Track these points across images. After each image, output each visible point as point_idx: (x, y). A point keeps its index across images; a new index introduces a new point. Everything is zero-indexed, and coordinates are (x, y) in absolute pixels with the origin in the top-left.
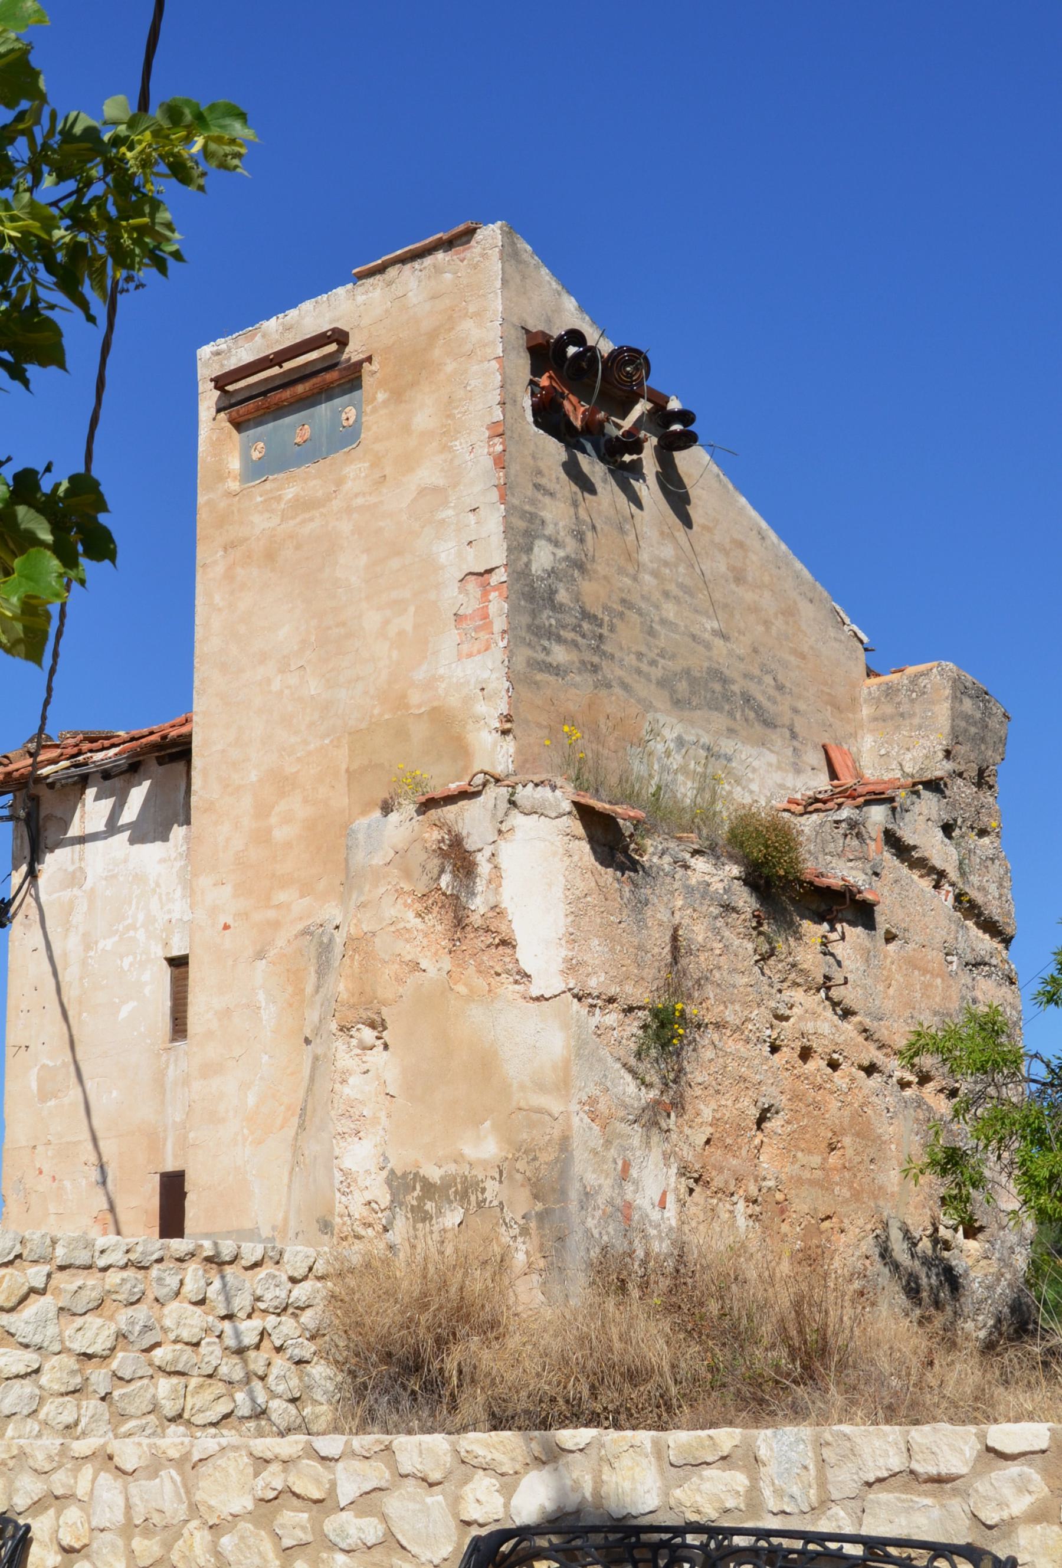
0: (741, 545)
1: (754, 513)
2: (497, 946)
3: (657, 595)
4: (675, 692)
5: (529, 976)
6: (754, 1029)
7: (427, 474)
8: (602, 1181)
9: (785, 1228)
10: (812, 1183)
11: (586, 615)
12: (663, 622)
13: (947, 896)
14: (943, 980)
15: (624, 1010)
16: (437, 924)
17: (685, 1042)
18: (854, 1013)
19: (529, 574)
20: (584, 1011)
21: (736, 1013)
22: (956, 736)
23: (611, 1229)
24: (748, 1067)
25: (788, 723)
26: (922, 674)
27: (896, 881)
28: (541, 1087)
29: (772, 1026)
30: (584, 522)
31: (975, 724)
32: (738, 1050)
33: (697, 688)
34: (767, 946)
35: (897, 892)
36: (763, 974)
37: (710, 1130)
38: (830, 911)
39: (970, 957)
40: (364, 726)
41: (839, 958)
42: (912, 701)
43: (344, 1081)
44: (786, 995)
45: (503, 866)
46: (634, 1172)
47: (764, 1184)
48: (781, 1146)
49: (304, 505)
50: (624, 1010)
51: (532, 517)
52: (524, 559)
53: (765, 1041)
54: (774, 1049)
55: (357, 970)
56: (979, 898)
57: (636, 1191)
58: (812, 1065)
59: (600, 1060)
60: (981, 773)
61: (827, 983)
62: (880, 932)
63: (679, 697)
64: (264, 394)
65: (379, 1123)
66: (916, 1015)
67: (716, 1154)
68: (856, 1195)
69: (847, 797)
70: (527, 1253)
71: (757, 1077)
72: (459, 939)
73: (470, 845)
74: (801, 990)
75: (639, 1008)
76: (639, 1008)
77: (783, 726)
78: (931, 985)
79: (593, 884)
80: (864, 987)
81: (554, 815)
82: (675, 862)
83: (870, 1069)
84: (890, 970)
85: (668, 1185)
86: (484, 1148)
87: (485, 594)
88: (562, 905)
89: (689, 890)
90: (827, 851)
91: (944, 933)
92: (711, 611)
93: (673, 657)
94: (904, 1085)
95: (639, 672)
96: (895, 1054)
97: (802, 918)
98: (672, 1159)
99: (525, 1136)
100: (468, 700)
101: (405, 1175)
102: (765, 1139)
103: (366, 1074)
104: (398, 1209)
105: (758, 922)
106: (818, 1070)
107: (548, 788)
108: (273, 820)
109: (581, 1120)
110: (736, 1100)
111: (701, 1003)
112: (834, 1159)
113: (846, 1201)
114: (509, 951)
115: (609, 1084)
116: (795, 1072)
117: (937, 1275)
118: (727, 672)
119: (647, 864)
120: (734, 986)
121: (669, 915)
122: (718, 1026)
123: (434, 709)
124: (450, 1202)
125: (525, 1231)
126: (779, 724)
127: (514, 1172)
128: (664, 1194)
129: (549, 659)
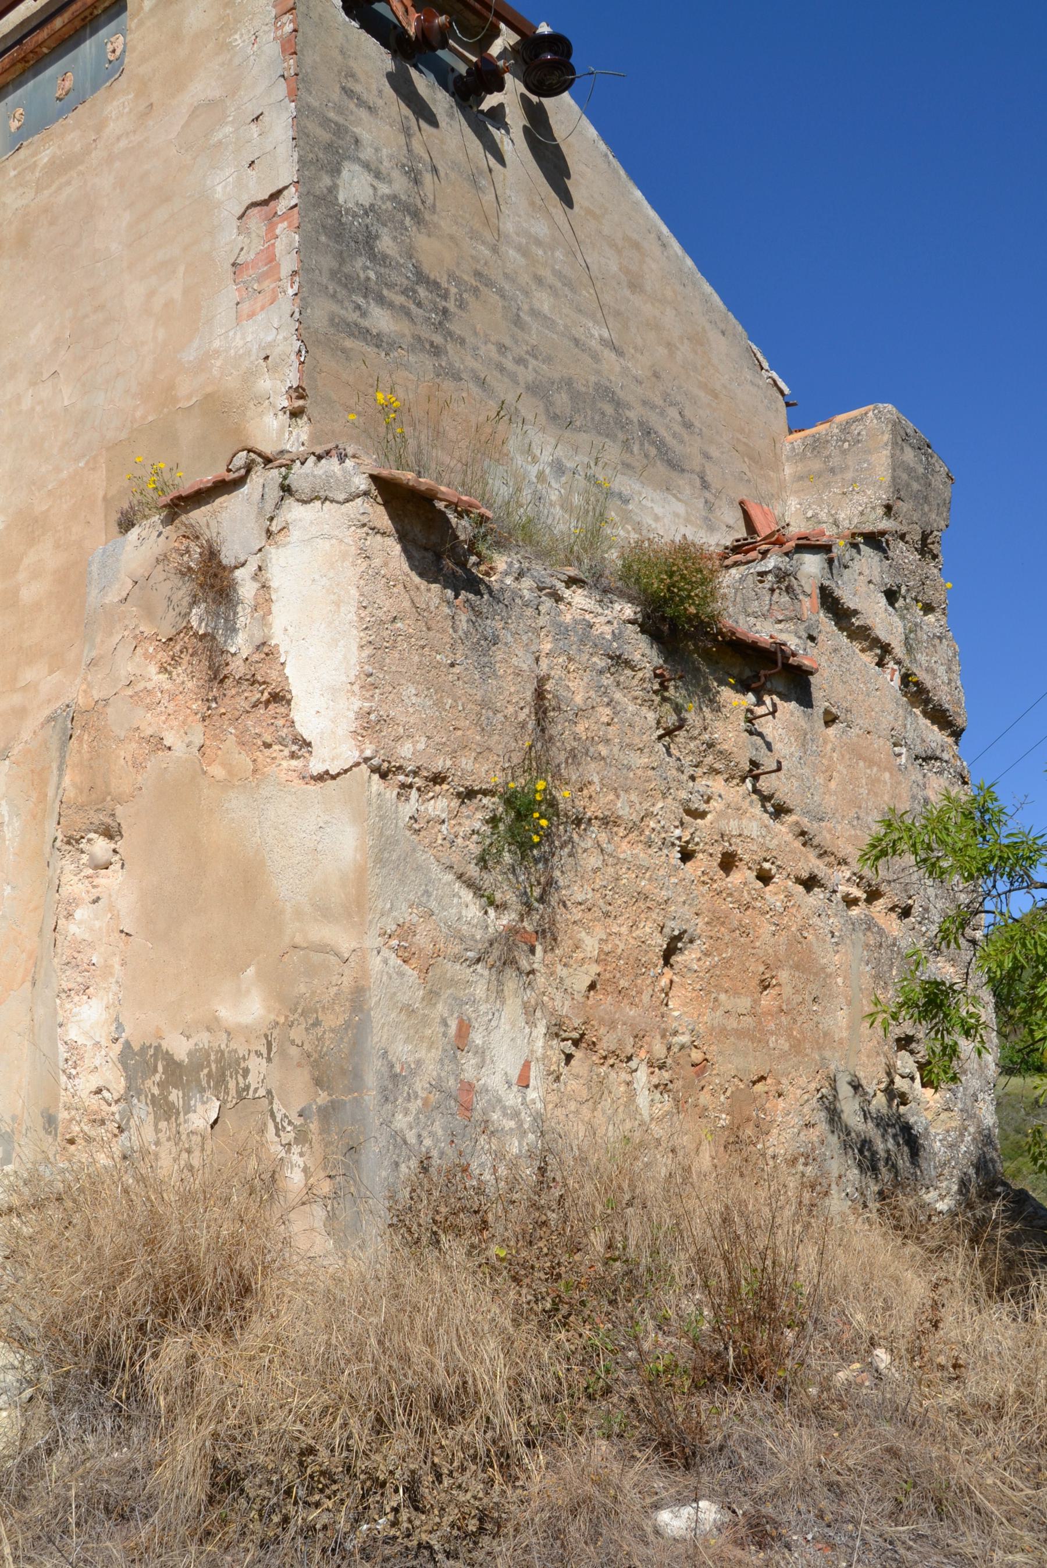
0: (636, 246)
1: (652, 213)
2: (267, 703)
3: (525, 278)
4: (552, 404)
5: (309, 745)
6: (658, 827)
7: (202, 87)
8: (422, 1054)
9: (704, 1098)
10: (740, 1034)
11: (421, 277)
12: (534, 313)
13: (893, 675)
14: (891, 774)
15: (459, 795)
16: (187, 679)
17: (557, 843)
18: (788, 811)
19: (335, 202)
20: (391, 794)
21: (632, 804)
22: (898, 490)
23: (438, 1128)
24: (650, 879)
25: (698, 469)
26: (856, 420)
27: (835, 650)
28: (324, 912)
29: (682, 824)
30: (420, 159)
31: (917, 479)
32: (635, 856)
33: (581, 405)
34: (675, 717)
35: (837, 666)
36: (669, 754)
37: (595, 969)
38: (757, 677)
39: (919, 750)
40: (123, 435)
41: (769, 739)
42: (844, 452)
43: (69, 916)
44: (701, 784)
45: (274, 584)
46: (477, 1038)
47: (675, 1040)
48: (698, 987)
49: (60, 167)
50: (459, 795)
51: (340, 131)
52: (327, 181)
53: (673, 844)
54: (687, 856)
55: (86, 756)
56: (929, 683)
57: (481, 1066)
58: (736, 877)
59: (418, 869)
60: (925, 537)
61: (754, 771)
62: (818, 711)
63: (558, 411)
64: (19, 42)
65: (112, 974)
66: (862, 815)
67: (604, 1002)
68: (797, 1047)
69: (773, 543)
70: (305, 1170)
71: (663, 893)
72: (215, 699)
73: (227, 558)
74: (720, 779)
75: (485, 793)
76: (485, 793)
77: (692, 472)
78: (878, 780)
79: (407, 604)
80: (800, 778)
81: (341, 497)
82: (541, 589)
83: (810, 883)
84: (831, 758)
85: (532, 1051)
86: (247, 1009)
87: (271, 226)
88: (355, 632)
89: (562, 631)
90: (750, 611)
91: (891, 718)
92: (599, 315)
93: (548, 360)
94: (850, 902)
95: (501, 369)
96: (839, 864)
97: (722, 682)
98: (538, 1014)
99: (302, 988)
100: (249, 377)
101: (144, 1049)
102: (675, 978)
103: (104, 899)
104: (135, 1101)
105: (661, 684)
106: (745, 884)
107: (335, 460)
108: (22, 576)
109: (386, 962)
110: (634, 925)
111: (581, 790)
112: (767, 1000)
113: (784, 1056)
114: (282, 710)
115: (433, 905)
116: (715, 886)
117: (895, 1136)
118: (620, 394)
119: (496, 586)
120: (629, 768)
121: (531, 660)
122: (605, 821)
123: (208, 397)
124: (202, 1090)
125: (302, 1136)
126: (687, 468)
127: (288, 1044)
128: (527, 1065)
129: (365, 323)
